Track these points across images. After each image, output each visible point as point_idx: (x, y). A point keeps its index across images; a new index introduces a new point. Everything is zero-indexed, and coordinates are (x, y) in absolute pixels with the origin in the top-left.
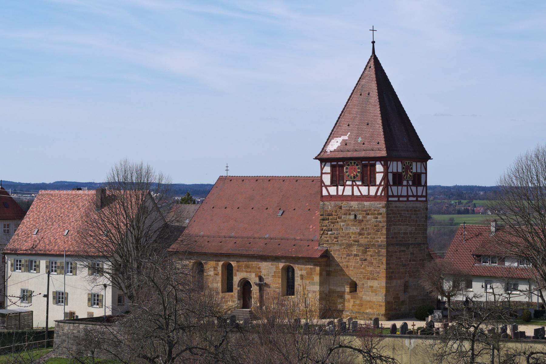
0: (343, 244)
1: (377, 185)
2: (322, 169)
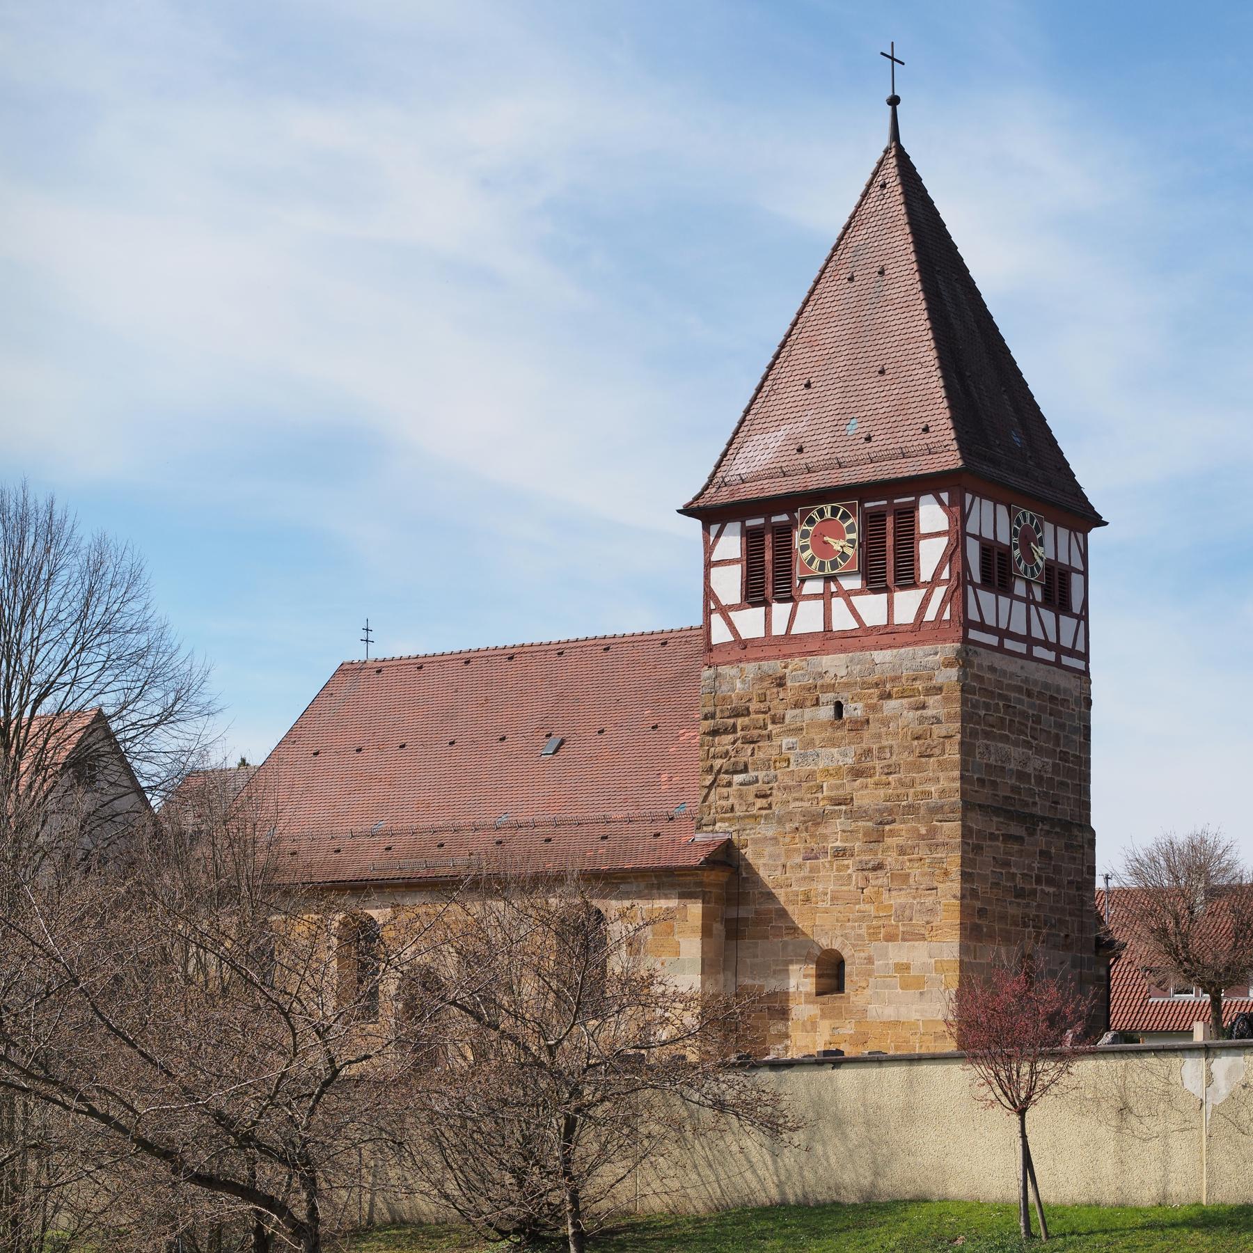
0: (790, 817)
2: (709, 549)
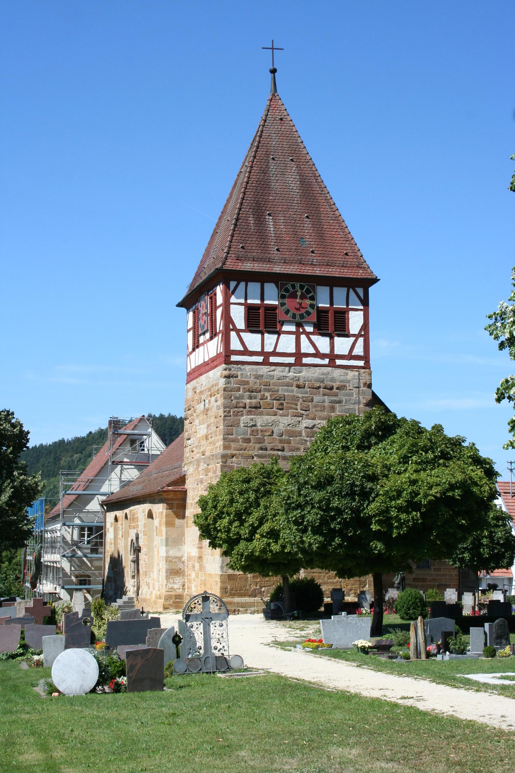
1: (354, 335)
